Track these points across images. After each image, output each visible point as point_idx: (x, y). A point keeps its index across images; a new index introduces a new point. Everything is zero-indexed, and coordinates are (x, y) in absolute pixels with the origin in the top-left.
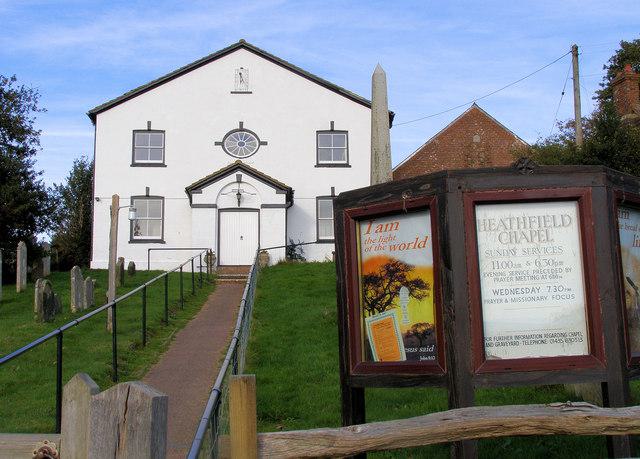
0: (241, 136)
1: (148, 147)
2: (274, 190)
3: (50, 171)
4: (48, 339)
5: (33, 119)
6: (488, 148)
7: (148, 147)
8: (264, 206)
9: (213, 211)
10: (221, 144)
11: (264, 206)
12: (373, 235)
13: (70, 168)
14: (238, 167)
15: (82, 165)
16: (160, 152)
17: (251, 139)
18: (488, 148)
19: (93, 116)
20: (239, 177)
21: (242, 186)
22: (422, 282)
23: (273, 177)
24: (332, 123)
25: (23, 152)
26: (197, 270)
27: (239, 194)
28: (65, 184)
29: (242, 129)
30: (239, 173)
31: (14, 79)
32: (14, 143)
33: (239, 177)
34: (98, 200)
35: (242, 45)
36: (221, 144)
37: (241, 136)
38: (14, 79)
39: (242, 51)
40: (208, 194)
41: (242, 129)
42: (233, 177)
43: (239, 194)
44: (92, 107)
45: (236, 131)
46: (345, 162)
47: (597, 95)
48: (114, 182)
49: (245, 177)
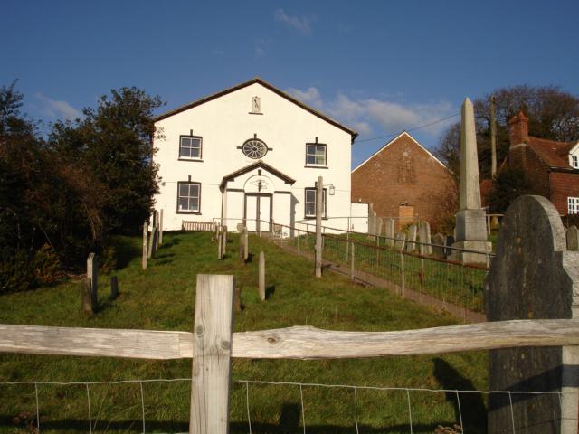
0: (253, 147)
2: (283, 182)
6: (412, 160)
8: (276, 192)
9: (242, 194)
10: (268, 149)
11: (276, 192)
12: (227, 280)
16: (196, 153)
17: (262, 146)
18: (412, 160)
20: (260, 172)
21: (261, 178)
22: (504, 92)
24: (317, 138)
26: (251, 226)
27: (260, 183)
29: (255, 139)
30: (260, 168)
33: (260, 172)
36: (268, 149)
40: (237, 183)
42: (255, 171)
43: (260, 183)
45: (251, 140)
47: (120, 94)
49: (264, 172)
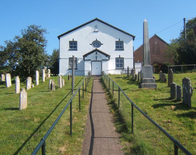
0: (97, 43)
1: (73, 45)
3: (49, 51)
4: (75, 74)
5: (45, 36)
7: (73, 45)
8: (103, 60)
11: (103, 60)
13: (128, 44)
14: (96, 50)
15: (55, 50)
19: (59, 37)
21: (97, 55)
23: (105, 52)
25: (43, 46)
28: (51, 55)
29: (96, 41)
30: (96, 52)
31: (40, 26)
32: (41, 43)
34: (60, 59)
35: (96, 19)
37: (97, 43)
38: (40, 26)
39: (96, 22)
40: (89, 57)
41: (96, 41)
42: (95, 53)
44: (59, 35)
46: (123, 68)
48: (65, 55)
49: (98, 53)
